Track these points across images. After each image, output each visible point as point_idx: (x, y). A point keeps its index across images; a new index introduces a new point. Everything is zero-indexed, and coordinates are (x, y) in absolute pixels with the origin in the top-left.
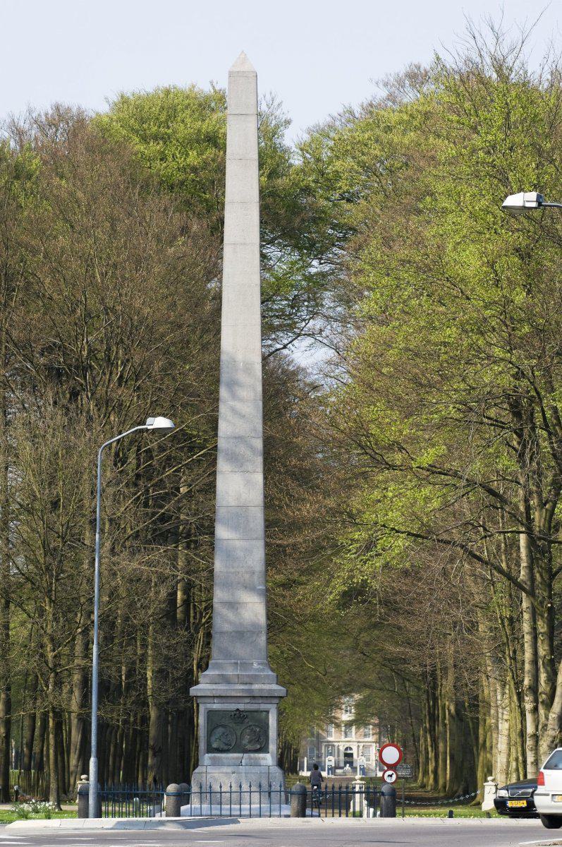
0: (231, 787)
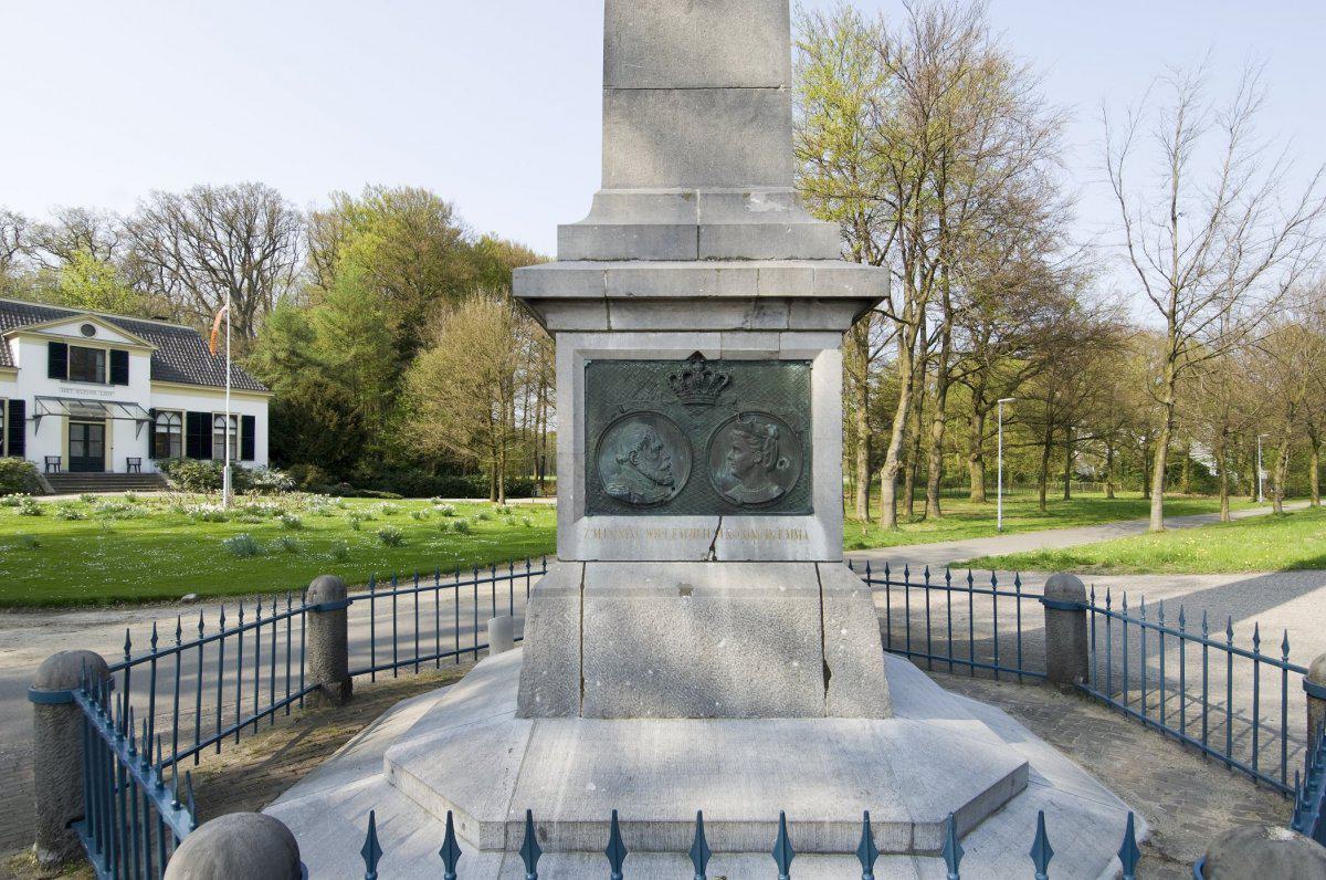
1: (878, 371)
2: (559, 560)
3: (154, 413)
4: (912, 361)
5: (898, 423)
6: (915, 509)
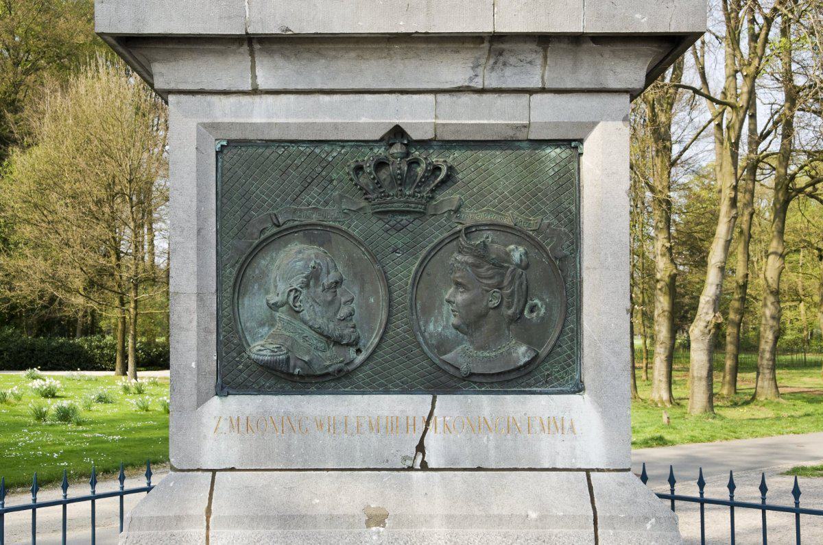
1: (683, 180)
2: (173, 469)
4: (735, 164)
5: (716, 255)
6: (739, 385)
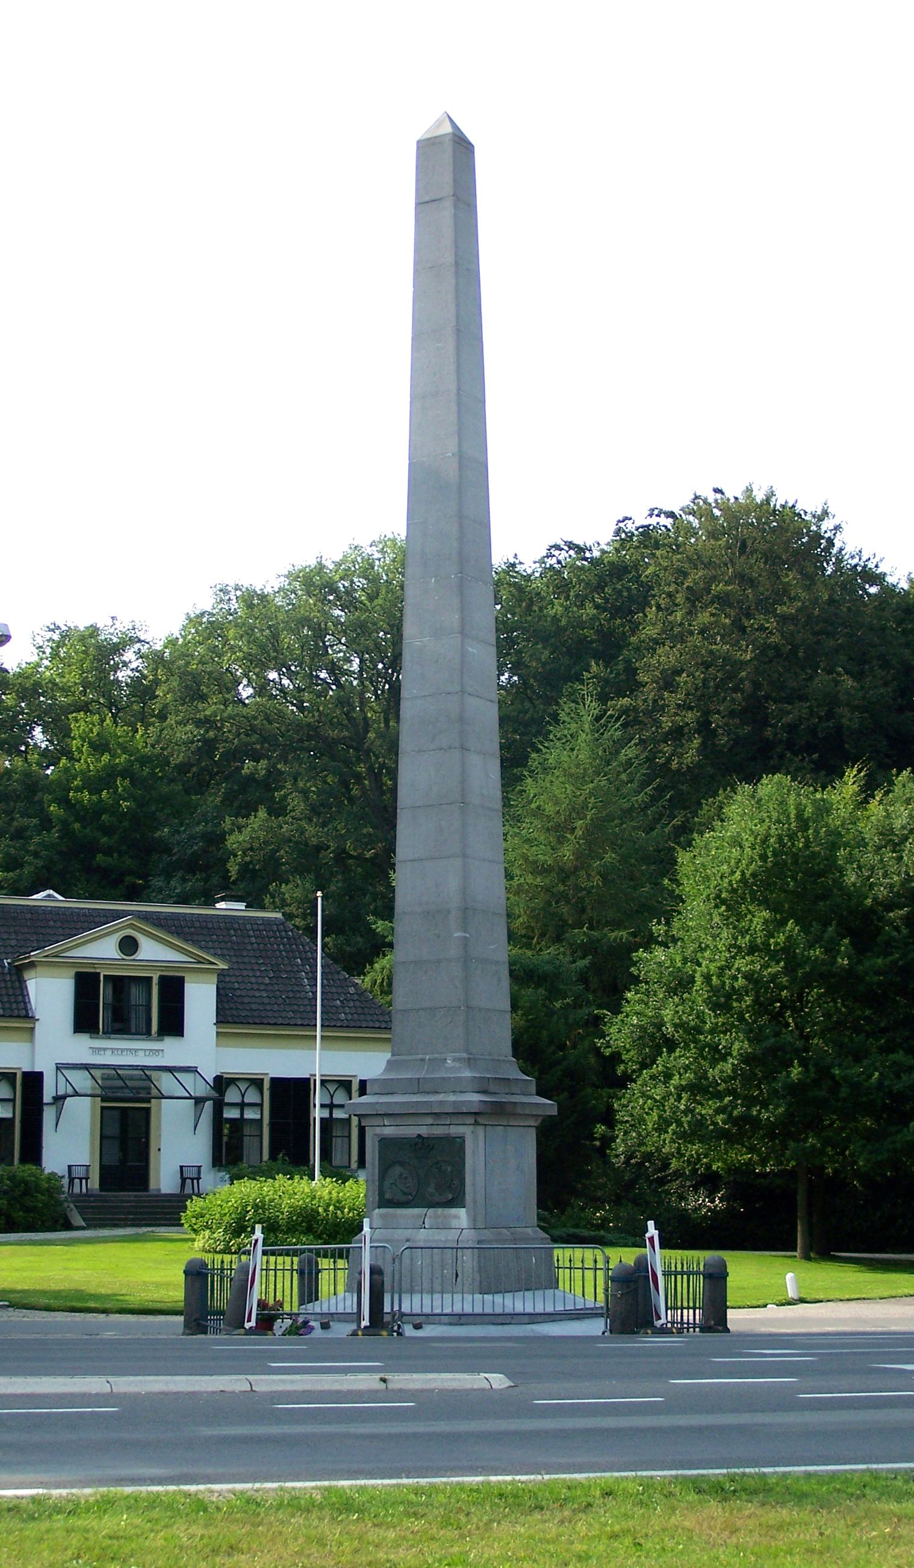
0: (596, 1261)
3: (221, 1083)
